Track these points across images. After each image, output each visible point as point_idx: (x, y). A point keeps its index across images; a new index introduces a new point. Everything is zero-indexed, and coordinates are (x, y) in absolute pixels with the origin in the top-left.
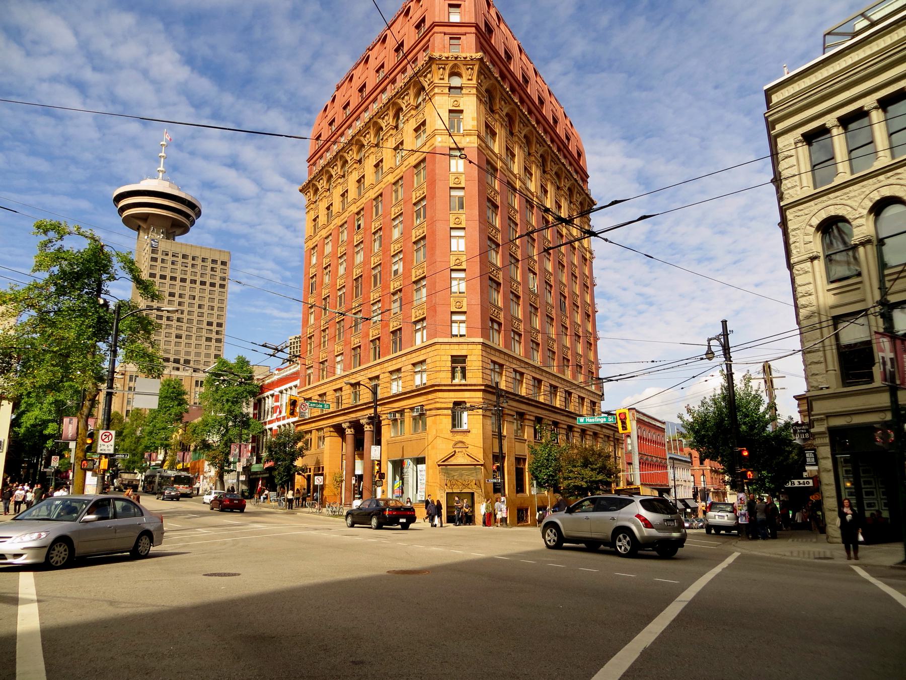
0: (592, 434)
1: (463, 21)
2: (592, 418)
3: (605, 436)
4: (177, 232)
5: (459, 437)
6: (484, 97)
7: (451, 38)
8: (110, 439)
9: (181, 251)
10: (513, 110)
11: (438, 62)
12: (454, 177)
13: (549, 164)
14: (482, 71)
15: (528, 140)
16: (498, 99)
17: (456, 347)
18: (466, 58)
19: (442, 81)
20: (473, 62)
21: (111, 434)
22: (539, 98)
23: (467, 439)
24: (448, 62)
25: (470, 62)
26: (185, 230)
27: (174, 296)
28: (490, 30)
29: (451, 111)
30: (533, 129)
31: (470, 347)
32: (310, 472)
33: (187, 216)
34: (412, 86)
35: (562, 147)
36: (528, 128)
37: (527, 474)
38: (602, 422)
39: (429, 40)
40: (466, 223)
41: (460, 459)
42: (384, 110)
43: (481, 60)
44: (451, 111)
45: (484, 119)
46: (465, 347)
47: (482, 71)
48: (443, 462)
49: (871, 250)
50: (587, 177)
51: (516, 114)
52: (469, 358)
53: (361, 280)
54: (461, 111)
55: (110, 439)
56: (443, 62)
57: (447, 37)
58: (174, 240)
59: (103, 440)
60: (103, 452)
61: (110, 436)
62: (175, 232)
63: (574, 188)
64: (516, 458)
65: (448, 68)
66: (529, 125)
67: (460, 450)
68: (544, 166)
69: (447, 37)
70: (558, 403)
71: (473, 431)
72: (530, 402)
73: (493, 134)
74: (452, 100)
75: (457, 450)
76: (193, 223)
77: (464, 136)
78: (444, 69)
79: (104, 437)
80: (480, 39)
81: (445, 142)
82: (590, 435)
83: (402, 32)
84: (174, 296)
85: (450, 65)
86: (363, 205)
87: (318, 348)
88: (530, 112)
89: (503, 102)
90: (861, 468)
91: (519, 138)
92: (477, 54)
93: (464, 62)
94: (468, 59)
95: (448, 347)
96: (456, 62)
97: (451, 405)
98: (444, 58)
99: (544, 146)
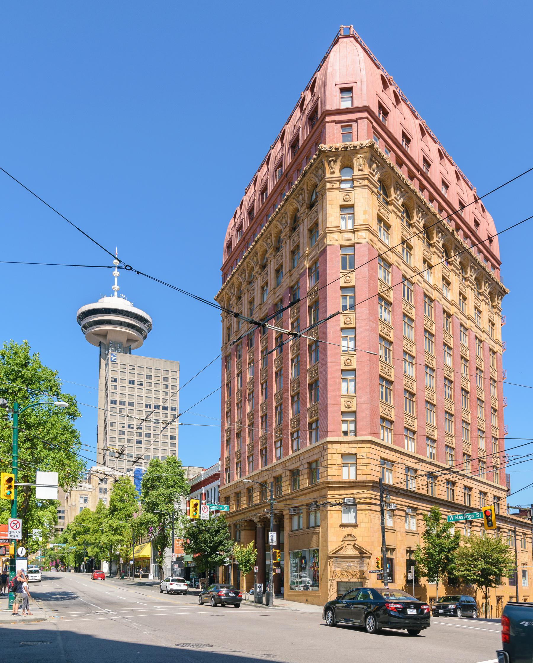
5: (348, 531)
6: (376, 187)
8: (18, 526)
10: (410, 198)
14: (398, 186)
15: (407, 211)
17: (347, 445)
18: (356, 147)
21: (18, 522)
22: (425, 160)
27: (124, 405)
28: (385, 113)
29: (342, 207)
30: (433, 217)
33: (139, 330)
41: (351, 551)
43: (372, 146)
44: (342, 207)
45: (422, 255)
47: (398, 186)
49: (353, 521)
53: (266, 385)
54: (352, 206)
55: (18, 526)
59: (12, 528)
60: (13, 538)
61: (18, 524)
66: (429, 213)
68: (428, 237)
70: (459, 499)
73: (388, 227)
74: (343, 195)
75: (347, 543)
77: (354, 232)
79: (12, 525)
80: (372, 123)
84: (124, 405)
87: (124, 453)
88: (412, 176)
91: (437, 248)
94: (358, 148)
95: (338, 446)
99: (446, 235)
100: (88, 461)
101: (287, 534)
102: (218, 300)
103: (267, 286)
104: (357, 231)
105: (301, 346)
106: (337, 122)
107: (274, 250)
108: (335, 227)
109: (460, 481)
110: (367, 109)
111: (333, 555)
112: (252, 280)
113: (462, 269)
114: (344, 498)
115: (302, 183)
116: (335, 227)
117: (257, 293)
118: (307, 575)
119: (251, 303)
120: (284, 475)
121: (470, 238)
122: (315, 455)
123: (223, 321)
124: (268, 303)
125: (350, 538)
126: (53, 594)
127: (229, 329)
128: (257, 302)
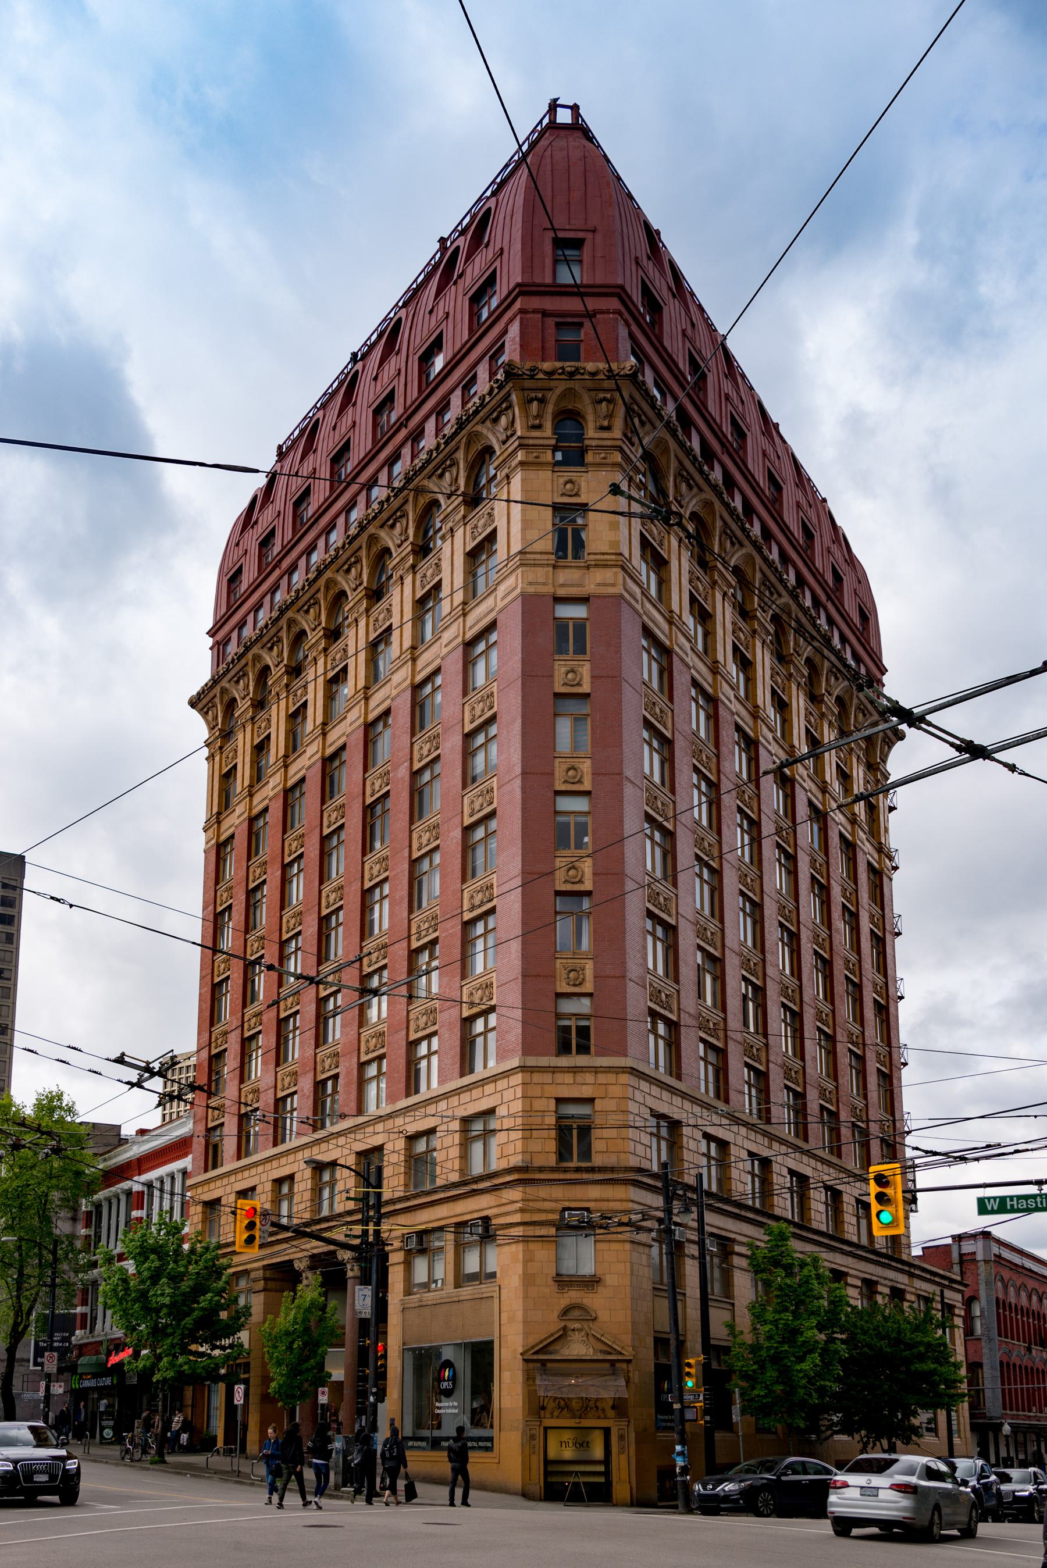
1: (598, 282)
3: (919, 1296)
5: (573, 1296)
7: (420, 906)
10: (708, 504)
11: (528, 384)
12: (565, 767)
16: (672, 479)
17: (568, 1078)
19: (536, 434)
23: (595, 1301)
24: (553, 384)
25: (607, 384)
30: (755, 553)
31: (602, 1078)
34: (462, 446)
35: (823, 597)
36: (744, 551)
39: (505, 332)
40: (553, 766)
41: (577, 1348)
42: (396, 503)
46: (589, 1078)
50: (883, 671)
51: (714, 513)
56: (540, 384)
57: (551, 322)
63: (851, 699)
64: (656, 1339)
65: (552, 397)
67: (577, 1325)
69: (551, 322)
71: (610, 1280)
72: (743, 1213)
74: (562, 480)
78: (542, 401)
81: (544, 584)
85: (558, 392)
89: (684, 486)
90: (559, 961)
93: (589, 384)
96: (570, 384)
98: (541, 376)
100: (545, 392)
101: (396, 1301)
102: (200, 705)
103: (388, 643)
104: (596, 566)
105: (390, 863)
106: (545, 314)
107: (368, 596)
108: (541, 553)
109: (779, 1159)
110: (620, 293)
111: (535, 1357)
112: (340, 626)
113: (739, 582)
114: (565, 1209)
115: (453, 443)
116: (541, 553)
117: (315, 695)
118: (130, 1435)
119: (261, 748)
120: (388, 1147)
122: (484, 1100)
123: (210, 758)
124: (349, 720)
125: (576, 1313)
126: (1029, 1211)
127: (228, 776)
128: (314, 715)
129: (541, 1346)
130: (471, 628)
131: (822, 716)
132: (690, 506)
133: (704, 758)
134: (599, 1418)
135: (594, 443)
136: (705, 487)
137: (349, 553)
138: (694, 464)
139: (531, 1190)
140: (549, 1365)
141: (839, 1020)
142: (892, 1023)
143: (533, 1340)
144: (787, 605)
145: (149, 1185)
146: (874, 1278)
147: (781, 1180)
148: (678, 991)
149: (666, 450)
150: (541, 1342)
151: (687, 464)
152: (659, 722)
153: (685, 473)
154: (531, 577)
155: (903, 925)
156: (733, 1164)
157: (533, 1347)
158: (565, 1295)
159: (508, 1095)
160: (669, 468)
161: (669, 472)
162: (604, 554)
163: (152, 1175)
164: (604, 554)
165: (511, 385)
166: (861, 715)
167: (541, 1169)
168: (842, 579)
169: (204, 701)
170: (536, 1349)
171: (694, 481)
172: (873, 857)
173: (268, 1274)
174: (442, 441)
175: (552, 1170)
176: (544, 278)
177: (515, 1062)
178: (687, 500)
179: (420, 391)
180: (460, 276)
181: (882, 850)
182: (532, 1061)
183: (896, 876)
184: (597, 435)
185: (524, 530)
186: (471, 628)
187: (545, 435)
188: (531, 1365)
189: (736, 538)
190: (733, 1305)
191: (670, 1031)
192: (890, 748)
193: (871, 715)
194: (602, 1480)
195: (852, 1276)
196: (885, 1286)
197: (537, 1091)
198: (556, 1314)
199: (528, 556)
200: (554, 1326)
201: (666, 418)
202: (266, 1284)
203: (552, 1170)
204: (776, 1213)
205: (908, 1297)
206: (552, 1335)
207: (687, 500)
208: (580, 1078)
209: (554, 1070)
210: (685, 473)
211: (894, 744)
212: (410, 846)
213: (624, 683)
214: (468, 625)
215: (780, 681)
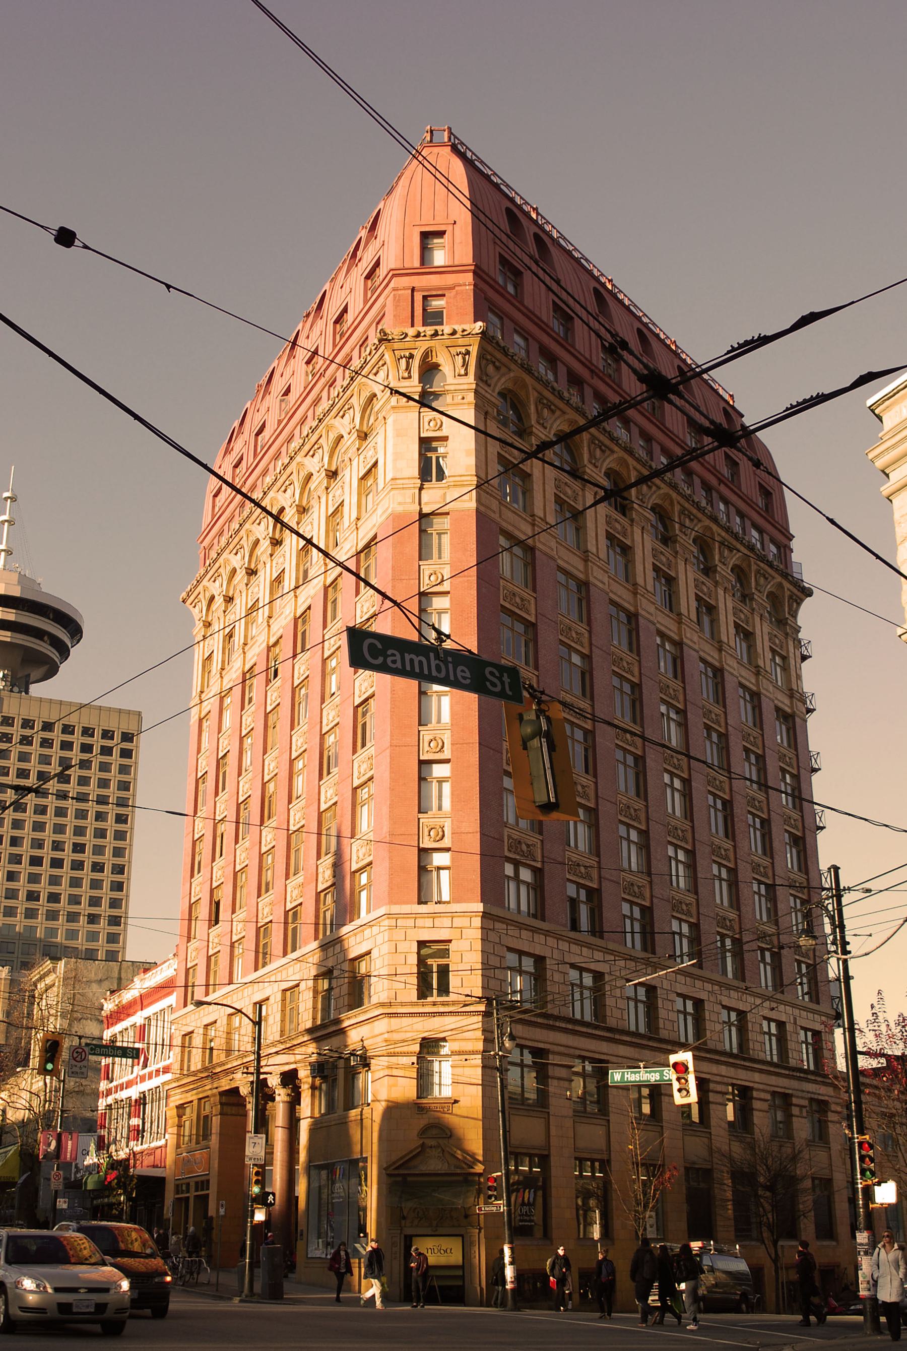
0: (805, 1103)
1: (456, 263)
2: (635, 1073)
4: (34, 675)
9: (40, 716)
11: (396, 346)
13: (532, 408)
16: (532, 408)
20: (466, 341)
26: (52, 671)
30: (627, 457)
32: (188, 1191)
36: (615, 456)
37: (860, 1193)
38: (653, 1079)
48: (396, 1168)
50: (790, 537)
52: (452, 947)
58: (27, 692)
59: (74, 1059)
62: (29, 675)
67: (433, 1143)
72: (617, 1037)
76: (64, 652)
82: (801, 1107)
83: (346, 289)
86: (281, 630)
92: (473, 325)
93: (448, 343)
97: (416, 1048)
100: (411, 351)
111: (396, 1172)
121: (718, 492)
122: (364, 943)
125: (434, 1132)
129: (401, 1162)
130: (362, 539)
131: (716, 583)
132: (555, 426)
133: (574, 635)
134: (453, 1226)
135: (452, 388)
136: (568, 410)
137: (284, 477)
138: (553, 393)
139: (395, 1021)
140: (410, 1179)
141: (740, 853)
142: (809, 852)
143: (394, 1158)
144: (667, 495)
145: (149, 1018)
146: (790, 1092)
147: (668, 1005)
148: (542, 841)
149: (525, 386)
150: (401, 1158)
151: (547, 394)
152: (521, 609)
153: (545, 401)
154: (400, 499)
155: (822, 762)
156: (608, 993)
157: (394, 1163)
158: (424, 1116)
159: (380, 939)
160: (528, 398)
161: (529, 402)
162: (461, 476)
163: (149, 1011)
164: (461, 476)
165: (383, 347)
166: (762, 580)
167: (402, 1004)
168: (738, 464)
169: (192, 598)
170: (398, 1164)
171: (554, 405)
172: (784, 703)
173: (224, 1099)
174: (341, 390)
175: (412, 1004)
176: (413, 262)
177: (382, 911)
178: (550, 422)
179: (335, 346)
180: (360, 261)
181: (796, 695)
182: (396, 909)
183: (812, 720)
184: (456, 381)
185: (395, 460)
186: (362, 539)
187: (412, 384)
188: (393, 1179)
189: (605, 446)
190: (609, 1121)
191: (535, 877)
192: (799, 604)
193: (773, 578)
194: (460, 1283)
195: (758, 1090)
196: (802, 1098)
197: (399, 935)
198: (415, 1132)
199: (398, 482)
200: (414, 1142)
201: (519, 361)
202: (222, 1109)
203: (412, 1004)
204: (661, 1036)
205: (833, 1107)
206: (411, 1152)
207: (550, 422)
208: (420, 922)
209: (416, 916)
210: (545, 401)
211: (802, 600)
212: (321, 722)
213: (789, 498)
214: (360, 537)
215: (664, 560)
